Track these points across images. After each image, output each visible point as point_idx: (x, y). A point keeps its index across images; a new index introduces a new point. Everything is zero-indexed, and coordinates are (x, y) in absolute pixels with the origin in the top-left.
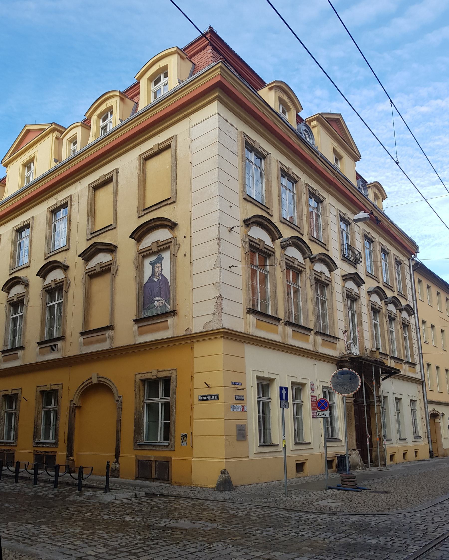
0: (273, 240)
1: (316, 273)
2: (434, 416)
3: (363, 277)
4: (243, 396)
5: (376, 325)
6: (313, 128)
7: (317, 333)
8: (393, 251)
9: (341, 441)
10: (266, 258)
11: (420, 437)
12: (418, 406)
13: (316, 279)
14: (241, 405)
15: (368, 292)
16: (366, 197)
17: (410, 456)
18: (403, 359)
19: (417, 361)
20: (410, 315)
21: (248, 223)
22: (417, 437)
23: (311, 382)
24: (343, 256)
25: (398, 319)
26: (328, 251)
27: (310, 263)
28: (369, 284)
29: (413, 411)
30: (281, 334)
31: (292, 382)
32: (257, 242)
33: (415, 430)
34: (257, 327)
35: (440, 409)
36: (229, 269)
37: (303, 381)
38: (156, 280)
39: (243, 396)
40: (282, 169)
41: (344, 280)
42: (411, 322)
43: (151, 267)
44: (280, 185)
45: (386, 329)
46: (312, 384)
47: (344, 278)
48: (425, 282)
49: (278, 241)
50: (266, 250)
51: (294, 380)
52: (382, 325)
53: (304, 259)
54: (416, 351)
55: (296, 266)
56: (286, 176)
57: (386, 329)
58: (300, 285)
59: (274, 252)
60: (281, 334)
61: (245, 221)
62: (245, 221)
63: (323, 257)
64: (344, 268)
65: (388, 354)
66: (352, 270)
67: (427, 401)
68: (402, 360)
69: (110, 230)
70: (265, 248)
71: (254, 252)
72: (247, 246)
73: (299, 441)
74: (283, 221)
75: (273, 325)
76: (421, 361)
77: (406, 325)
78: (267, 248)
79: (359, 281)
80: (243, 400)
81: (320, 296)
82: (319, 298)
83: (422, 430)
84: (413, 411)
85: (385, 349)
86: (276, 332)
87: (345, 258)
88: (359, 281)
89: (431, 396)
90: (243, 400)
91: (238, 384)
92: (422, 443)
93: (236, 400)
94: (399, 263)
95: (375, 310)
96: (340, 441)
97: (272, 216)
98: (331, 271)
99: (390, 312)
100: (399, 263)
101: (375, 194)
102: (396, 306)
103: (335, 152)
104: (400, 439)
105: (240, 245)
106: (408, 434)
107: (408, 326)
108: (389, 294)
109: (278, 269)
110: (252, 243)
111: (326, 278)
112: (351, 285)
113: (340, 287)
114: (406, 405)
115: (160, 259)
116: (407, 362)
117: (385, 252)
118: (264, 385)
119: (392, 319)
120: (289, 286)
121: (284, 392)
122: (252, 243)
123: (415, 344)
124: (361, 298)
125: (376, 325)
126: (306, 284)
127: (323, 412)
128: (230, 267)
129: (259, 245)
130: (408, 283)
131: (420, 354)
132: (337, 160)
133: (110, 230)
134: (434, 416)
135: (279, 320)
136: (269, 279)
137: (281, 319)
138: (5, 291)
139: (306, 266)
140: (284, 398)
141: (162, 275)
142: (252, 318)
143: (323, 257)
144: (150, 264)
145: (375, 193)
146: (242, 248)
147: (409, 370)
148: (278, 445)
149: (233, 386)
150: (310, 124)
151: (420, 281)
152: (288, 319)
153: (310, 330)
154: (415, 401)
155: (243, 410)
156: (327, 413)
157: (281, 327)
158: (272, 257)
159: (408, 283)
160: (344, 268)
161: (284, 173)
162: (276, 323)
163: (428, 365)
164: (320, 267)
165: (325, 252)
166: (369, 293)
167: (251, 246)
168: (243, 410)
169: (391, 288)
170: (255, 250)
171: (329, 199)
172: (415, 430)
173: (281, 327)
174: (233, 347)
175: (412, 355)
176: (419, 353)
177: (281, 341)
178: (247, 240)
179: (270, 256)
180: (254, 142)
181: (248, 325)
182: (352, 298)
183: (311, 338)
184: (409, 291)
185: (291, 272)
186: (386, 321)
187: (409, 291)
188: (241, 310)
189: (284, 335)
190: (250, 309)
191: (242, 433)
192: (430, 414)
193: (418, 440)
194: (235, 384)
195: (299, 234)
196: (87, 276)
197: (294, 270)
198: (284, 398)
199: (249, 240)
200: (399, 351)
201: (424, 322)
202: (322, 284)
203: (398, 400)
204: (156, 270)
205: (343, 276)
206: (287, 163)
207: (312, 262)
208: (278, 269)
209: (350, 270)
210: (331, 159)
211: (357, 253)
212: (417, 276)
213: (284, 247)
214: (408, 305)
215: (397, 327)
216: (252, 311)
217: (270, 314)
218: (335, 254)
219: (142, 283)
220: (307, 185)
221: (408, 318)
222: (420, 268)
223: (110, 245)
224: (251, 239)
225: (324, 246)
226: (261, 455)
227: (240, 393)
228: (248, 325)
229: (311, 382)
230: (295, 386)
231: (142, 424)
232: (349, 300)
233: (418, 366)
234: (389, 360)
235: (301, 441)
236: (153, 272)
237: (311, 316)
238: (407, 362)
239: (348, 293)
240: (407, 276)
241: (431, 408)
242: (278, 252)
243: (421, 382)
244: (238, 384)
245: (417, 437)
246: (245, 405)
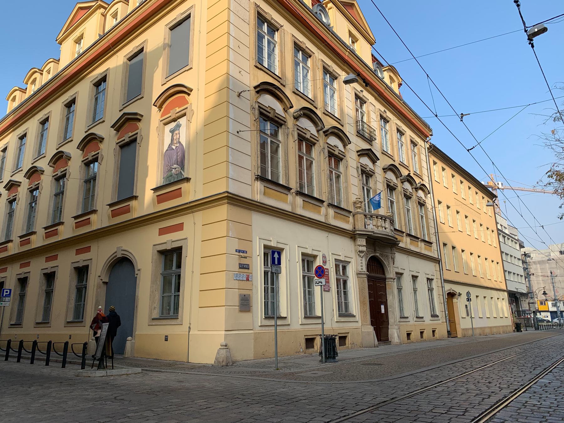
0: (285, 110)
1: (300, 128)
2: (451, 295)
3: (378, 154)
4: (248, 265)
5: (392, 202)
6: (329, 9)
7: (331, 205)
8: (409, 133)
9: (355, 316)
10: (278, 127)
11: (438, 316)
12: (435, 285)
13: (329, 152)
14: (245, 274)
15: (383, 169)
16: (381, 80)
17: (428, 334)
18: (419, 237)
19: (433, 239)
20: (426, 195)
22: (434, 316)
23: (324, 254)
24: (357, 132)
25: (414, 197)
26: (343, 126)
27: (324, 136)
28: (383, 162)
29: (431, 290)
30: (294, 204)
31: (302, 253)
32: (268, 110)
33: (433, 308)
34: (264, 194)
35: (457, 289)
36: (237, 134)
37: (315, 253)
38: (174, 147)
39: (248, 265)
42: (427, 202)
43: (171, 134)
45: (401, 207)
46: (324, 257)
47: (359, 153)
48: (440, 164)
50: (277, 119)
51: (305, 251)
52: (398, 202)
53: (318, 131)
54: (432, 231)
55: (309, 137)
56: (266, 22)
57: (401, 207)
58: (313, 157)
59: (285, 122)
60: (294, 204)
63: (336, 131)
64: (359, 144)
65: (404, 230)
66: (367, 146)
67: (444, 280)
68: (418, 238)
69: (138, 99)
70: (276, 116)
71: (266, 121)
72: (257, 112)
73: (309, 314)
74: (296, 93)
75: (282, 194)
76: (438, 240)
77: (422, 204)
78: (277, 116)
79: (374, 159)
80: (248, 269)
81: (335, 170)
82: (334, 172)
83: (439, 309)
84: (431, 290)
85: (401, 227)
86: (285, 201)
87: (360, 134)
89: (448, 276)
90: (248, 269)
91: (243, 252)
92: (440, 322)
93: (240, 268)
94: (414, 144)
95: (391, 188)
96: (354, 316)
97: (284, 86)
98: (345, 146)
99: (405, 190)
100: (414, 144)
101: (391, 77)
102: (411, 184)
103: (351, 34)
104: (417, 317)
106: (425, 312)
107: (424, 205)
108: (405, 173)
109: (291, 139)
110: (261, 110)
111: (340, 152)
112: (365, 161)
113: (355, 162)
114: (422, 284)
115: (179, 126)
116: (424, 241)
117: (400, 132)
118: (273, 256)
119: (408, 197)
121: (276, 256)
122: (261, 110)
123: (432, 224)
124: (376, 174)
125: (392, 202)
126: (318, 156)
127: (320, 280)
128: (238, 132)
129: (270, 113)
130: (424, 164)
131: (437, 233)
132: (353, 42)
133: (138, 99)
134: (451, 295)
135: (289, 189)
136: (280, 148)
137: (291, 189)
138: (51, 166)
139: (320, 138)
140: (276, 263)
141: (180, 143)
142: (259, 185)
143: (336, 131)
144: (170, 131)
145: (390, 77)
146: (252, 114)
147: (425, 249)
148: (286, 318)
149: (237, 253)
150: (327, 6)
151: (435, 163)
152: (299, 189)
153: (322, 202)
154: (432, 279)
155: (248, 280)
156: (323, 280)
158: (283, 126)
159: (424, 164)
160: (359, 144)
161: (298, 47)
162: (286, 192)
163: (445, 245)
164: (333, 141)
165: (393, 163)
166: (385, 170)
167: (261, 114)
168: (248, 280)
169: (406, 167)
170: (264, 115)
172: (433, 308)
173: (290, 198)
174: (241, 214)
175: (429, 234)
176: (435, 233)
177: (291, 211)
178: (257, 106)
179: (281, 125)
181: (256, 192)
182: (367, 174)
183: (323, 210)
184: (425, 172)
185: (304, 143)
186: (402, 200)
187: (425, 172)
188: (248, 177)
189: (293, 205)
190: (258, 176)
191: (245, 304)
192: (448, 294)
193: (436, 318)
194: (239, 251)
195: (337, 123)
196: (118, 147)
197: (306, 142)
198: (276, 263)
199: (259, 106)
200: (416, 230)
201: (440, 203)
202: (335, 158)
203: (415, 278)
204: (175, 138)
205: (357, 152)
206: (301, 38)
207: (326, 136)
208: (291, 139)
209: (365, 146)
210: (348, 41)
211: (372, 130)
212: (432, 158)
214: (423, 185)
215: (412, 205)
216: (262, 178)
217: (281, 183)
218: (350, 130)
219: (162, 151)
221: (424, 198)
222: (434, 151)
223: (136, 114)
224: (261, 106)
225: (339, 121)
226: (267, 328)
227: (244, 261)
228: (256, 192)
229: (324, 254)
230: (306, 258)
232: (364, 176)
233: (434, 245)
234: (404, 238)
235: (313, 315)
236: (172, 140)
237: (325, 188)
238: (424, 241)
239: (363, 169)
240: (423, 157)
241: (448, 287)
242: (290, 122)
243: (437, 261)
244: (243, 252)
245: (434, 316)
246: (251, 275)
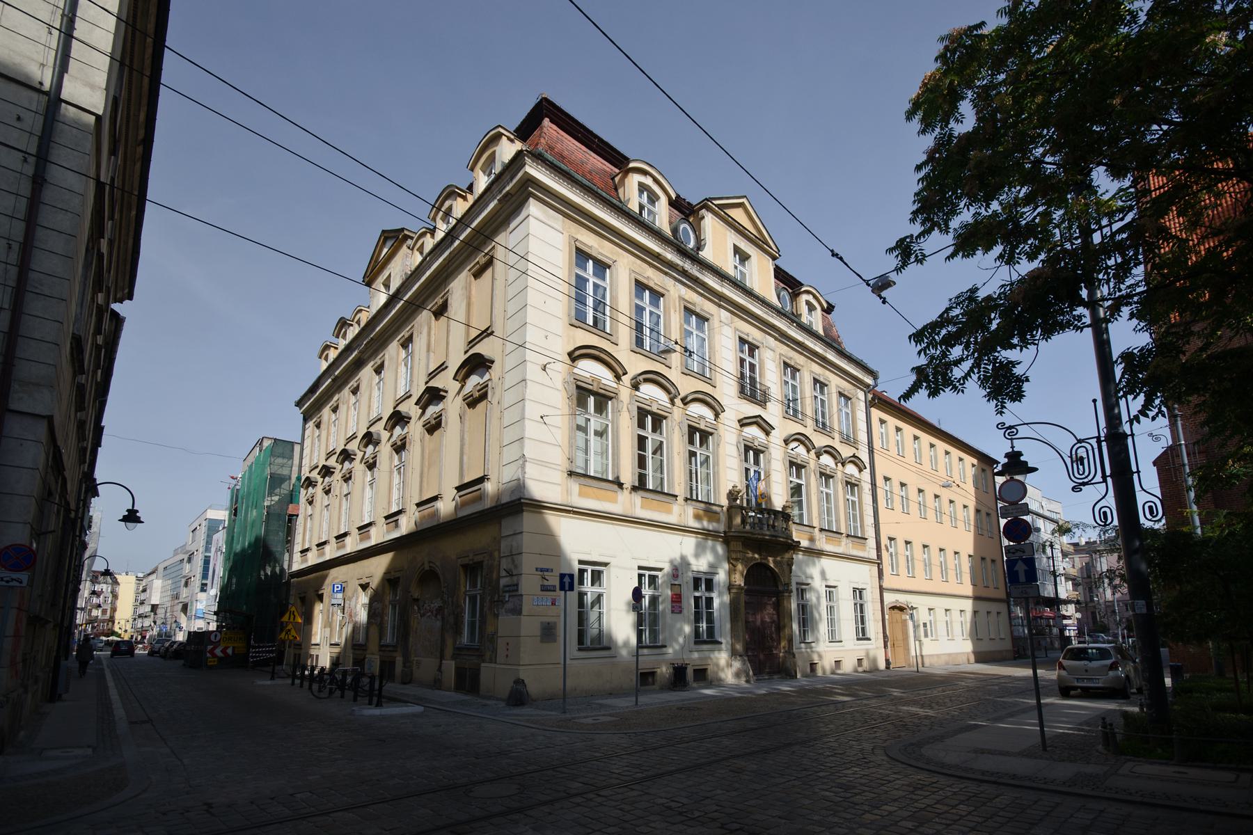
21: (574, 356)
40: (637, 281)
41: (742, 426)
44: (839, 403)
49: (813, 452)
61: (570, 354)
62: (570, 354)
88: (767, 429)
98: (768, 434)
105: (560, 387)
120: (747, 470)
142: (575, 486)
147: (580, 494)
157: (844, 540)
165: (707, 388)
167: (578, 387)
171: (720, 316)
180: (590, 247)
188: (559, 476)
194: (542, 570)
202: (698, 435)
213: (818, 455)
220: (681, 298)
231: (462, 622)
